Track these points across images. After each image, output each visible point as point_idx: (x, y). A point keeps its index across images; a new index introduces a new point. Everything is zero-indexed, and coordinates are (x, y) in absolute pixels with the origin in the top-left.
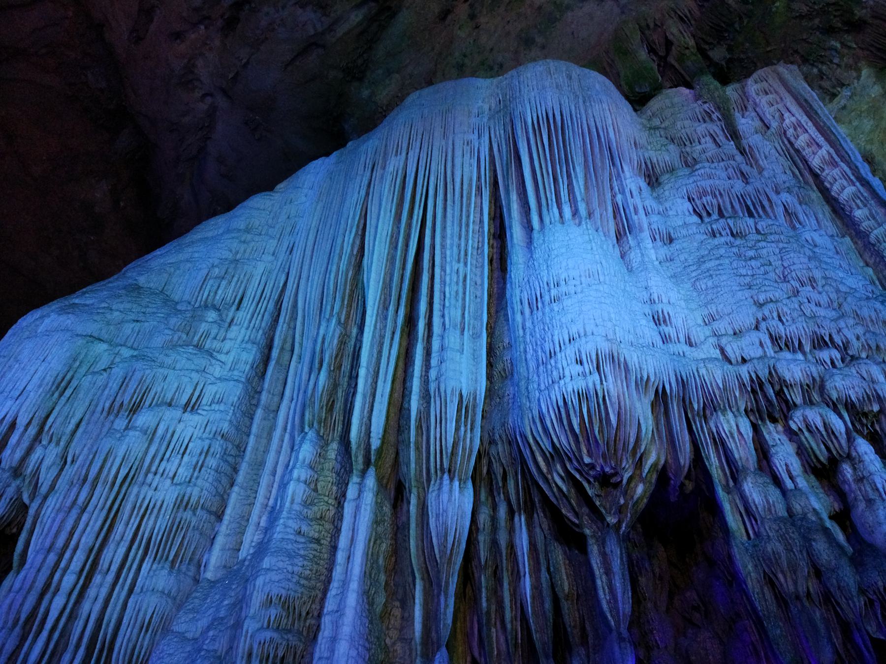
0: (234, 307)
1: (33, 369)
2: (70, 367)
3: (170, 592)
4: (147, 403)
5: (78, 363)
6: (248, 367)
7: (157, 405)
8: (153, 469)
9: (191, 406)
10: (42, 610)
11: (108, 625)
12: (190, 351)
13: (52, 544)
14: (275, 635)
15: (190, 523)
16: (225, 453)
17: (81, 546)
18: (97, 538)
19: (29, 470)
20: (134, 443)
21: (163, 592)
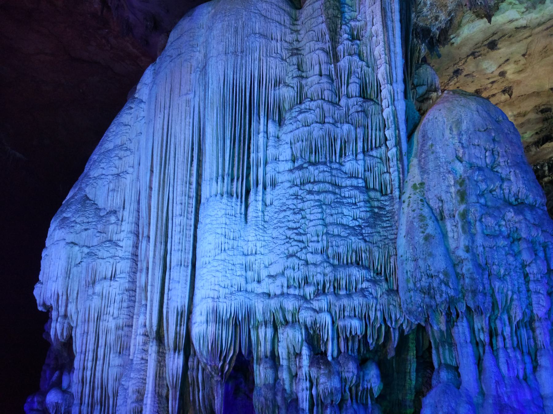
0: (122, 209)
1: (57, 264)
2: (68, 262)
3: (121, 364)
4: (97, 281)
5: (70, 260)
6: (131, 248)
7: (101, 280)
8: (105, 312)
9: (113, 277)
10: (85, 377)
11: (105, 379)
12: (107, 245)
13: (82, 351)
14: (136, 404)
15: (122, 334)
16: (130, 296)
17: (90, 350)
18: (95, 344)
19: (69, 315)
20: (96, 302)
21: (118, 366)
